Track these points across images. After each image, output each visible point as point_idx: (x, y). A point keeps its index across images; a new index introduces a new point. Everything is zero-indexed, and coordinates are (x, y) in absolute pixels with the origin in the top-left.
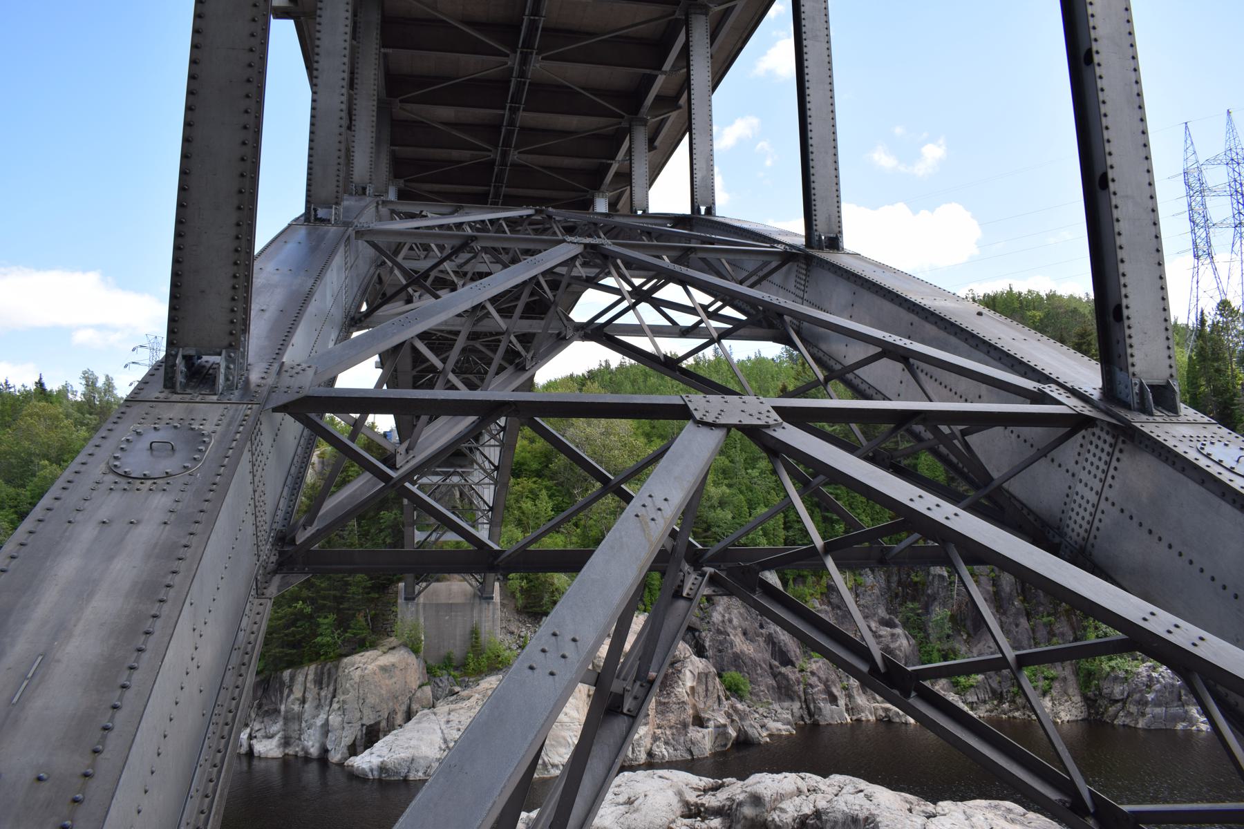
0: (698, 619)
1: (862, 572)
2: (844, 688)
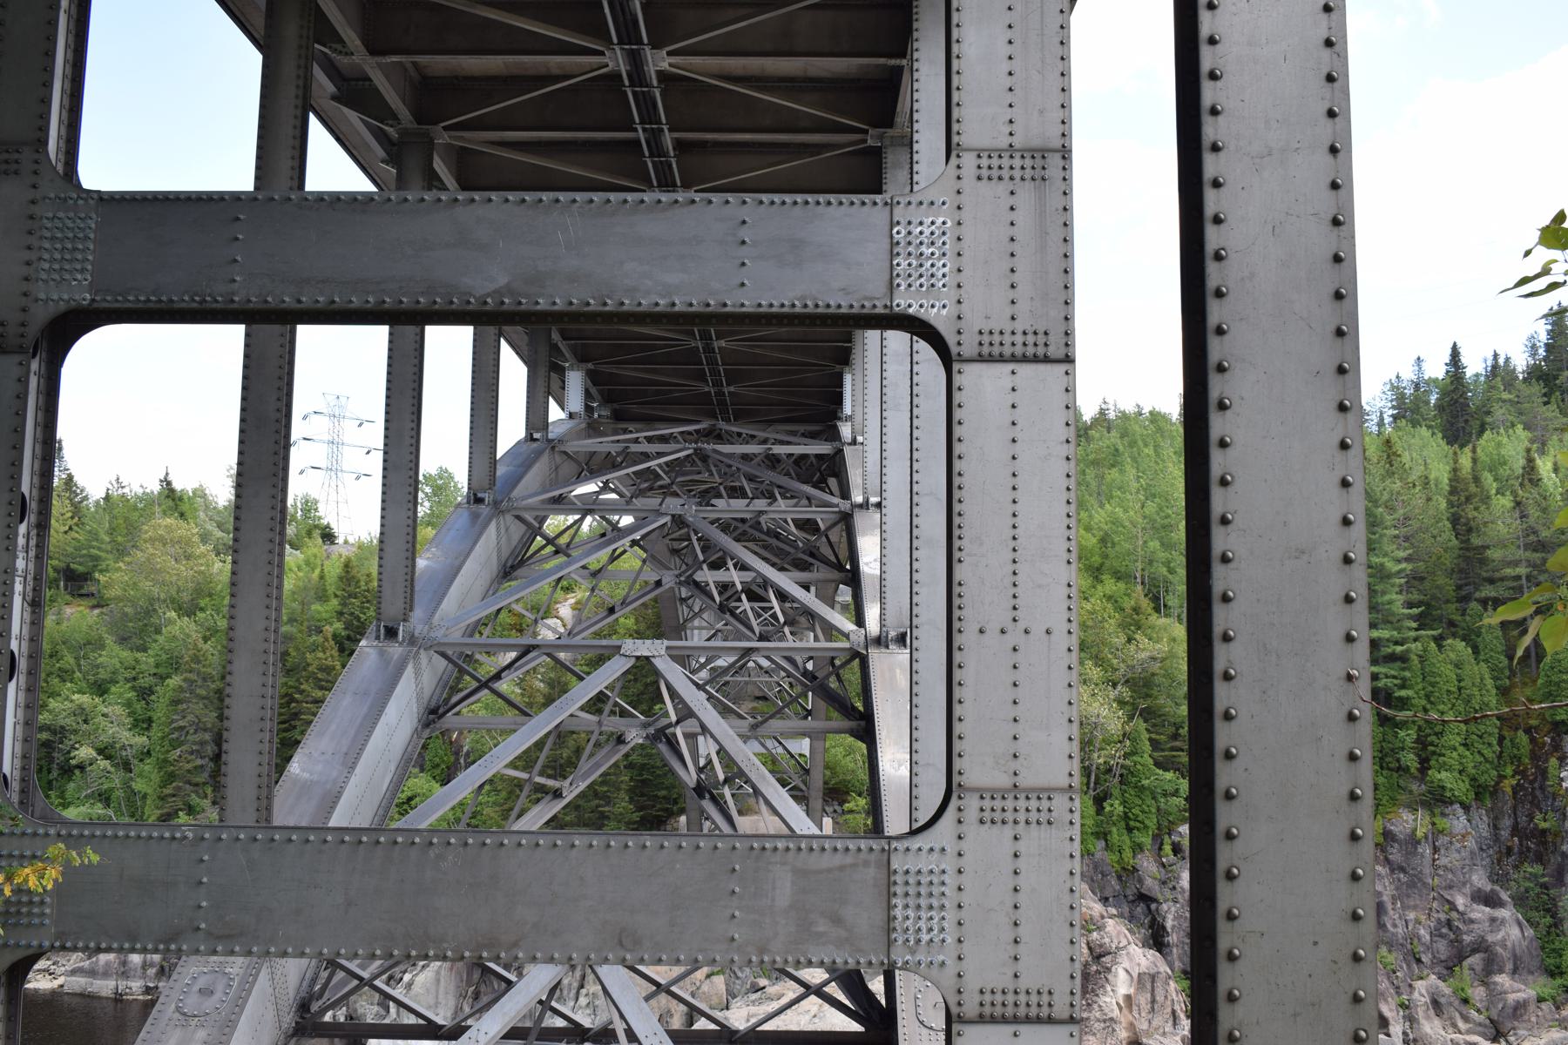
0: (1156, 882)
1: (1447, 811)
2: (1402, 1006)
